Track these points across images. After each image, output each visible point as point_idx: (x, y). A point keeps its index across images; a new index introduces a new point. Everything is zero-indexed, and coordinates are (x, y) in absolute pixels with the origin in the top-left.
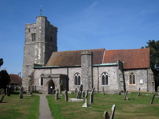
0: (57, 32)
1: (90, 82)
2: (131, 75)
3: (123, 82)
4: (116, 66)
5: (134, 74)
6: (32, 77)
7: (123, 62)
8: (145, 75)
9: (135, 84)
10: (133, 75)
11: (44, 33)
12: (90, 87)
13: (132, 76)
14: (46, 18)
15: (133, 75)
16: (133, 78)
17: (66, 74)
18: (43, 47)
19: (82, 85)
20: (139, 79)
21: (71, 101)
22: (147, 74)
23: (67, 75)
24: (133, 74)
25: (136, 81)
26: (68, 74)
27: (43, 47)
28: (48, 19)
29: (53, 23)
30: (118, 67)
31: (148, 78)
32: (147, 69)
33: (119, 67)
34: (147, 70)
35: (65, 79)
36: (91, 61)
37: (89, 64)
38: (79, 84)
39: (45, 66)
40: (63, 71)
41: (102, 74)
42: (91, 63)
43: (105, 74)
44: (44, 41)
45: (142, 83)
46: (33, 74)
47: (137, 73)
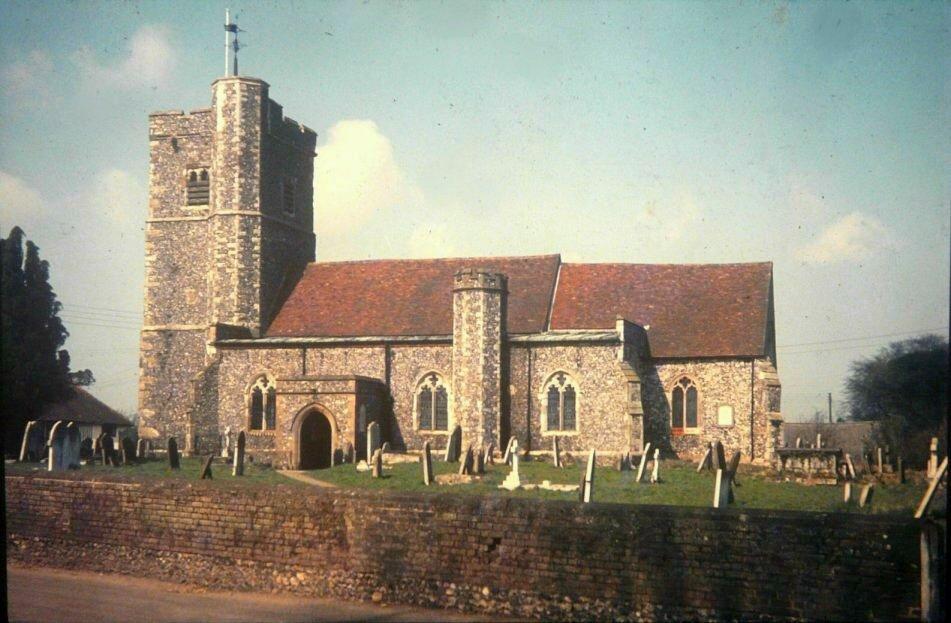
0: (557, 258)
1: (493, 416)
2: (681, 386)
3: (641, 418)
4: (613, 342)
5: (691, 384)
6: (209, 383)
7: (647, 328)
8: (744, 387)
9: (695, 426)
10: (689, 386)
11: (258, 166)
12: (493, 436)
13: (685, 391)
14: (264, 88)
15: (689, 386)
16: (688, 401)
17: (378, 375)
18: (254, 239)
19: (458, 432)
20: (716, 406)
21: (887, 454)
22: (753, 385)
23: (384, 381)
24: (689, 381)
25: (700, 416)
26: (388, 377)
27: (254, 239)
28: (272, 95)
29: (296, 110)
30: (620, 351)
31: (753, 403)
32: (753, 361)
33: (625, 351)
34: (753, 367)
35: (375, 399)
36: (498, 319)
37: (488, 333)
38: (442, 422)
39: (263, 332)
40: (367, 363)
41: (550, 379)
42: (498, 329)
43: (561, 380)
44: (255, 209)
45: (729, 422)
46: (212, 371)
47: (707, 378)
